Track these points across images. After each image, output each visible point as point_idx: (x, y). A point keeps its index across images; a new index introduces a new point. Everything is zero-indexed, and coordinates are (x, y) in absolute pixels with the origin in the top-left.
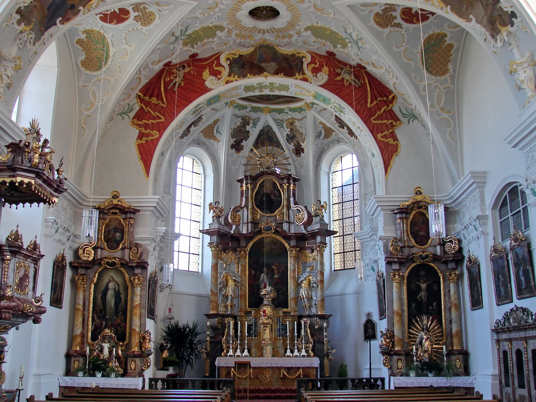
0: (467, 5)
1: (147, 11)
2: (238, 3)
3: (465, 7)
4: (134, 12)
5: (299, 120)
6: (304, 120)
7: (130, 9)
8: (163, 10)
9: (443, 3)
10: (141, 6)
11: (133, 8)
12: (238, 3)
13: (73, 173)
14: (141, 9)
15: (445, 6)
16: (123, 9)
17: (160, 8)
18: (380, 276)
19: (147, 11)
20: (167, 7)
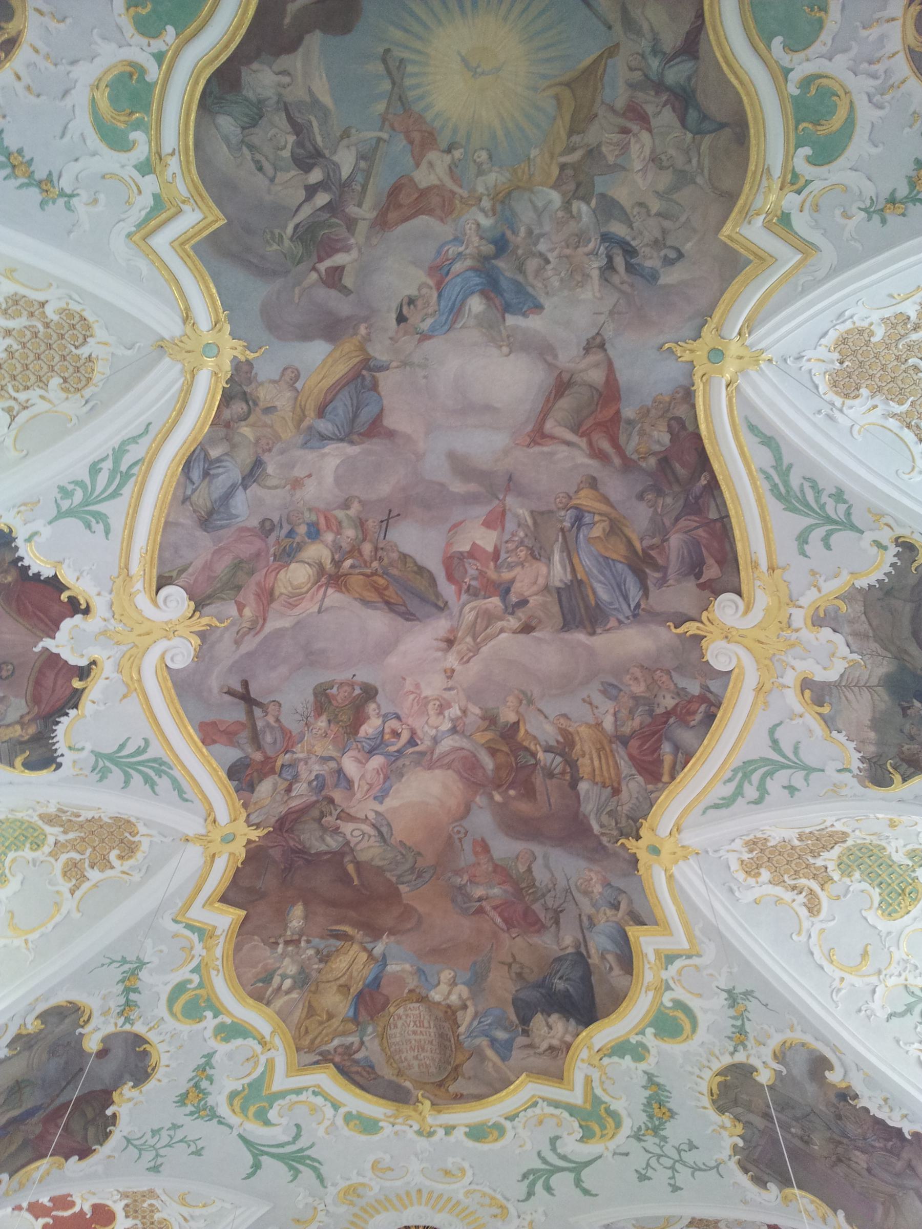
0: (883, 1204)
1: (157, 1216)
2: (376, 1205)
3: (880, 1211)
4: (127, 1217)
5: (850, 771)
6: (646, 665)
7: (118, 1208)
8: (192, 1217)
9: (824, 1205)
10: (144, 1201)
11: (127, 1205)
12: (376, 1205)
13: (190, 728)
14: (144, 1211)
15: (829, 1211)
16: (104, 1206)
17: (185, 1211)
18: (238, 868)
19: (157, 1216)
20: (204, 1211)
